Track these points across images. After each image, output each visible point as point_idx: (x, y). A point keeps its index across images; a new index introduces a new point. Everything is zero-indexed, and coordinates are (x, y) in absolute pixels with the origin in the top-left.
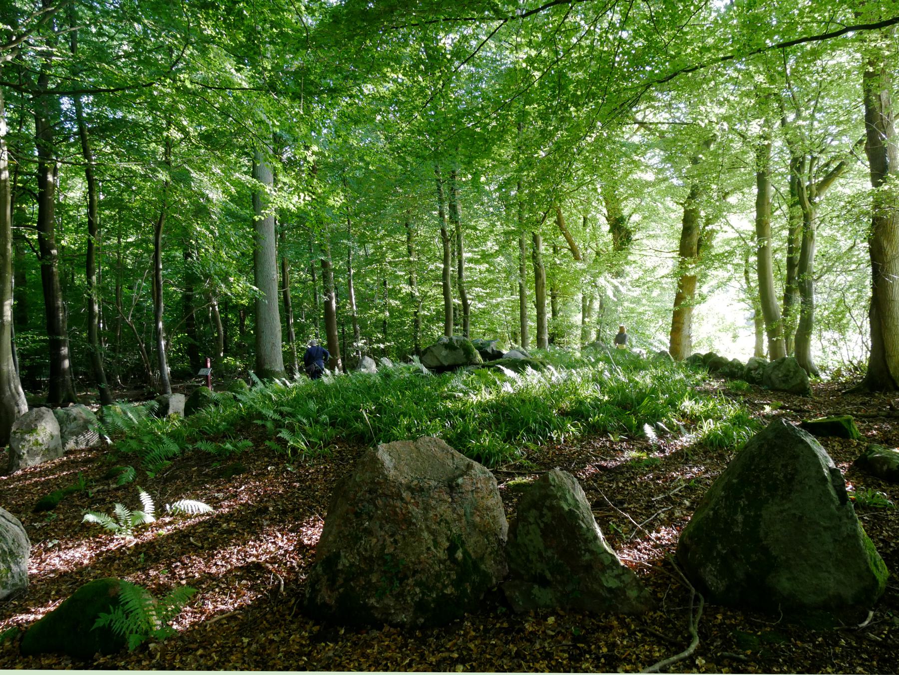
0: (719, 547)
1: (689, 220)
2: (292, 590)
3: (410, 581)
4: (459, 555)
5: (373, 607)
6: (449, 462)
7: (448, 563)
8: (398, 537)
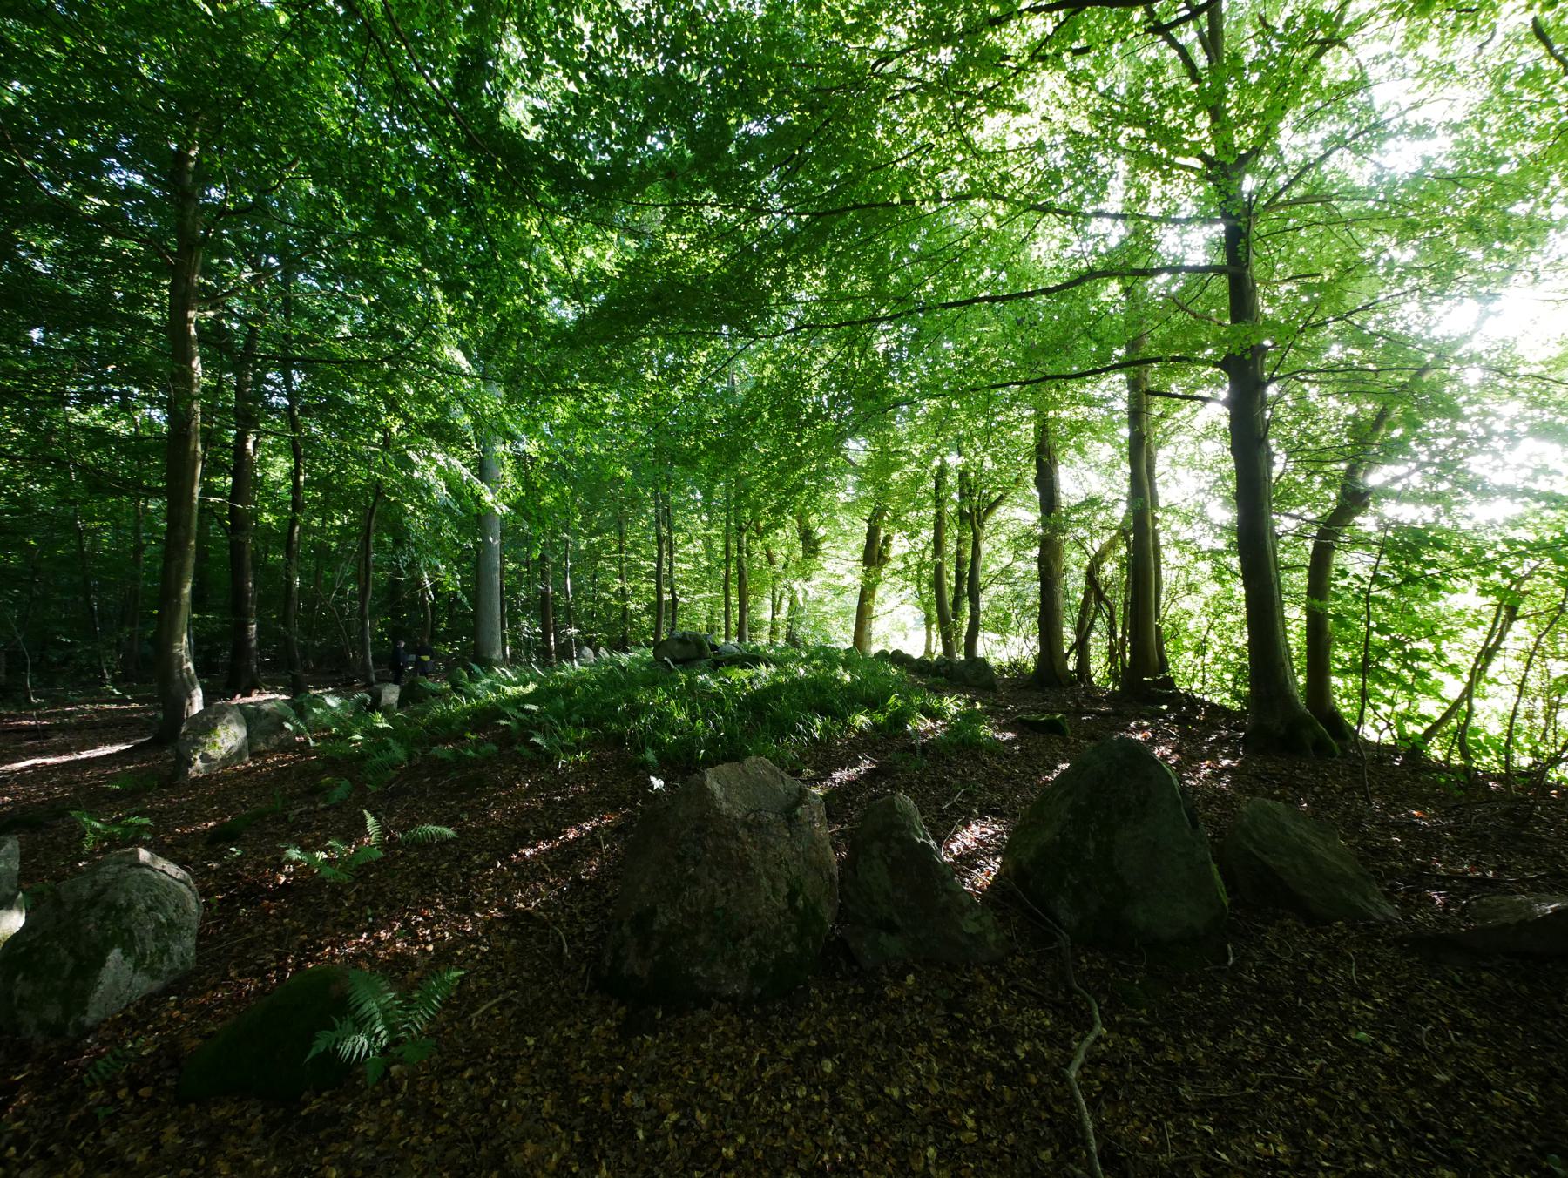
0: (1070, 876)
1: (872, 535)
2: (579, 951)
3: (747, 941)
4: (800, 903)
5: (698, 977)
6: (781, 787)
7: (789, 914)
8: (731, 886)
